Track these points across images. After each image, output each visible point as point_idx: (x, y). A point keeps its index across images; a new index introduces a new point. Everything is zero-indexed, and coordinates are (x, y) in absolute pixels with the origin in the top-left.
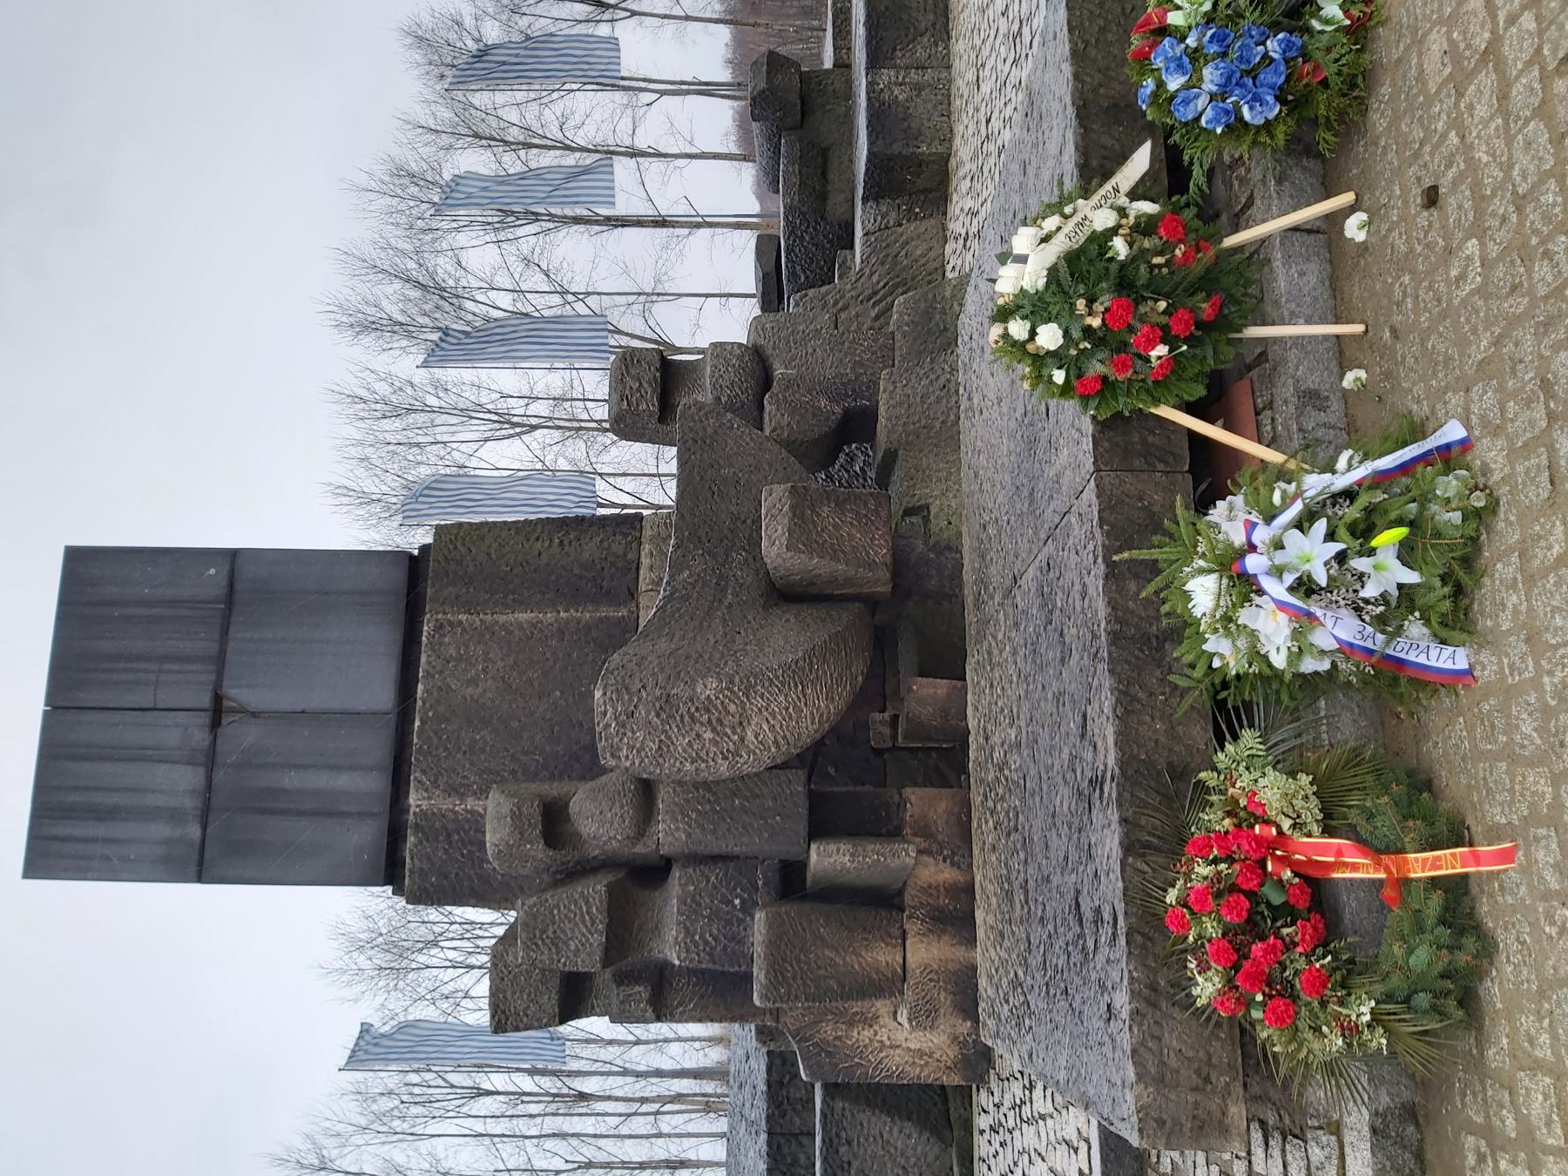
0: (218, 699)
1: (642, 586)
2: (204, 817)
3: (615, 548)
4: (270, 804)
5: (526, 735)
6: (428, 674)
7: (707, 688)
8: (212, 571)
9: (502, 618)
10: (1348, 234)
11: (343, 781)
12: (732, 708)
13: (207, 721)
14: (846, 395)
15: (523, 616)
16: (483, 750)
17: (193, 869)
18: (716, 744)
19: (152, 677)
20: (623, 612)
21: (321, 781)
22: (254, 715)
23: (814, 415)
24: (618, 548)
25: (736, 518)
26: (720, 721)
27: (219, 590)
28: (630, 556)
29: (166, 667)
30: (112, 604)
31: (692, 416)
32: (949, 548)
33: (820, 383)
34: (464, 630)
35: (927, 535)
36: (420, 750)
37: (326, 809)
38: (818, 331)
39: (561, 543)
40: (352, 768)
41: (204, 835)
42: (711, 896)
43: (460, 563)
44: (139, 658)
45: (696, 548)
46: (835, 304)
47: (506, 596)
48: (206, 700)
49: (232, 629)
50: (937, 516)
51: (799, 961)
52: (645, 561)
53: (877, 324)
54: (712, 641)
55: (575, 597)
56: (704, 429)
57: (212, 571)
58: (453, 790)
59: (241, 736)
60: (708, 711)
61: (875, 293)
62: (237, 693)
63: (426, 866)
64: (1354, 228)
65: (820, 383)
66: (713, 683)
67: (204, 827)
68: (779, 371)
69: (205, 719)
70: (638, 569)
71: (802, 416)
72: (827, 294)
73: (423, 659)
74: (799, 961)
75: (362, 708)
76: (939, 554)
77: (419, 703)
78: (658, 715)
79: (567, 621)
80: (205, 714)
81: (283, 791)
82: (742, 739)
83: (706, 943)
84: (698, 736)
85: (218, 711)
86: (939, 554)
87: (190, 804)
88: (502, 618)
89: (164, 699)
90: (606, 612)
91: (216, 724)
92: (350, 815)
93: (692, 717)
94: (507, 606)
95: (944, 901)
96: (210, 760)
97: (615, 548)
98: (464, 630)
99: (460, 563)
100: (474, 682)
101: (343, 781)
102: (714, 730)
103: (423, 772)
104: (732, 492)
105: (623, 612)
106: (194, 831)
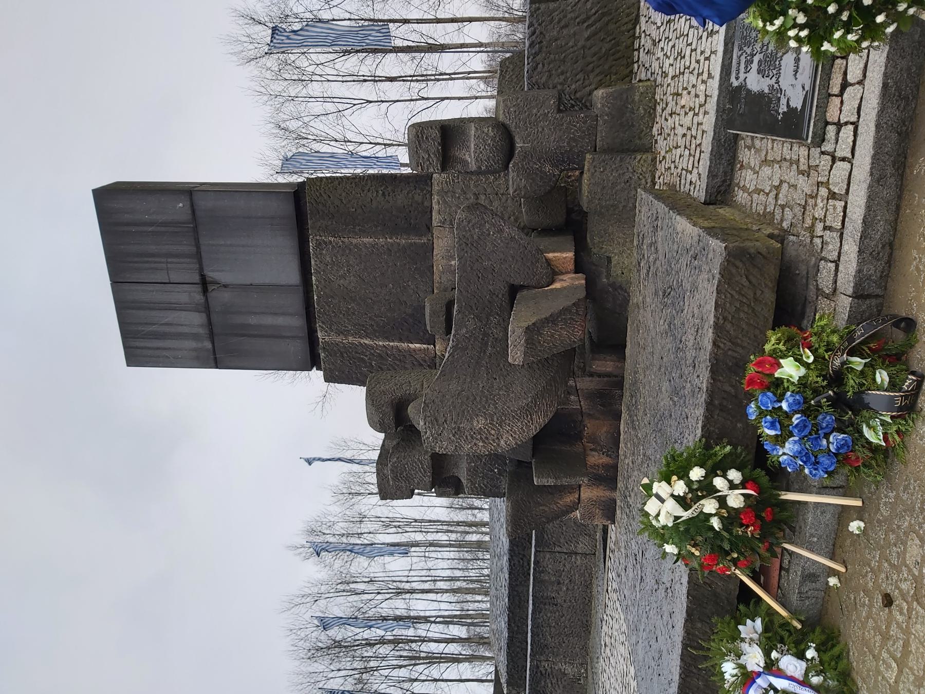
0: (203, 278)
1: (435, 223)
2: (212, 336)
3: (417, 197)
4: (245, 331)
5: (376, 307)
6: (317, 272)
7: (479, 423)
8: (181, 205)
9: (354, 241)
10: (851, 524)
11: (280, 321)
12: (493, 432)
13: (200, 289)
14: (563, 161)
15: (366, 240)
16: (354, 314)
17: (213, 365)
18: (485, 447)
19: (164, 265)
20: (424, 240)
21: (269, 320)
22: (225, 286)
23: (541, 178)
24: (418, 198)
25: (492, 294)
26: (487, 438)
27: (186, 216)
28: (426, 204)
29: (169, 260)
30: (128, 224)
31: (464, 227)
32: (621, 287)
33: (546, 153)
34: (333, 247)
35: (609, 275)
36: (319, 312)
37: (275, 334)
38: (546, 115)
39: (383, 194)
40: (283, 314)
41: (214, 346)
42: (483, 468)
43: (324, 205)
44: (153, 255)
45: (470, 313)
46: (559, 22)
47: (354, 228)
48: (196, 278)
49: (201, 241)
50: (615, 266)
51: (527, 516)
52: (435, 207)
53: (588, 44)
54: (481, 385)
55: (395, 230)
56: (472, 236)
57: (181, 205)
58: (339, 332)
59: (220, 297)
60: (480, 434)
61: (588, 18)
62: (211, 274)
63: (333, 367)
64: (855, 526)
65: (546, 153)
66: (482, 421)
67: (213, 343)
68: (519, 144)
69: (198, 288)
70: (431, 212)
71: (533, 179)
72: (554, 10)
73: (313, 262)
74: (527, 516)
75: (283, 283)
76: (615, 289)
77: (315, 287)
78: (454, 436)
79: (392, 245)
80: (192, 272)
81: (250, 325)
82: (498, 445)
83: (481, 488)
84: (475, 444)
85: (205, 284)
86: (615, 289)
87: (202, 331)
88: (354, 241)
89: (174, 277)
90: (415, 240)
91: (205, 291)
92: (288, 337)
93: (472, 437)
94: (356, 234)
95: (601, 472)
96: (207, 309)
97: (417, 197)
98: (333, 247)
99: (324, 205)
100: (343, 277)
101: (280, 321)
102: (483, 442)
103: (323, 323)
104: (490, 276)
105: (424, 240)
106: (208, 345)
